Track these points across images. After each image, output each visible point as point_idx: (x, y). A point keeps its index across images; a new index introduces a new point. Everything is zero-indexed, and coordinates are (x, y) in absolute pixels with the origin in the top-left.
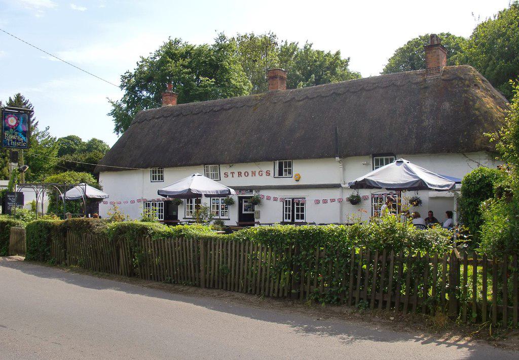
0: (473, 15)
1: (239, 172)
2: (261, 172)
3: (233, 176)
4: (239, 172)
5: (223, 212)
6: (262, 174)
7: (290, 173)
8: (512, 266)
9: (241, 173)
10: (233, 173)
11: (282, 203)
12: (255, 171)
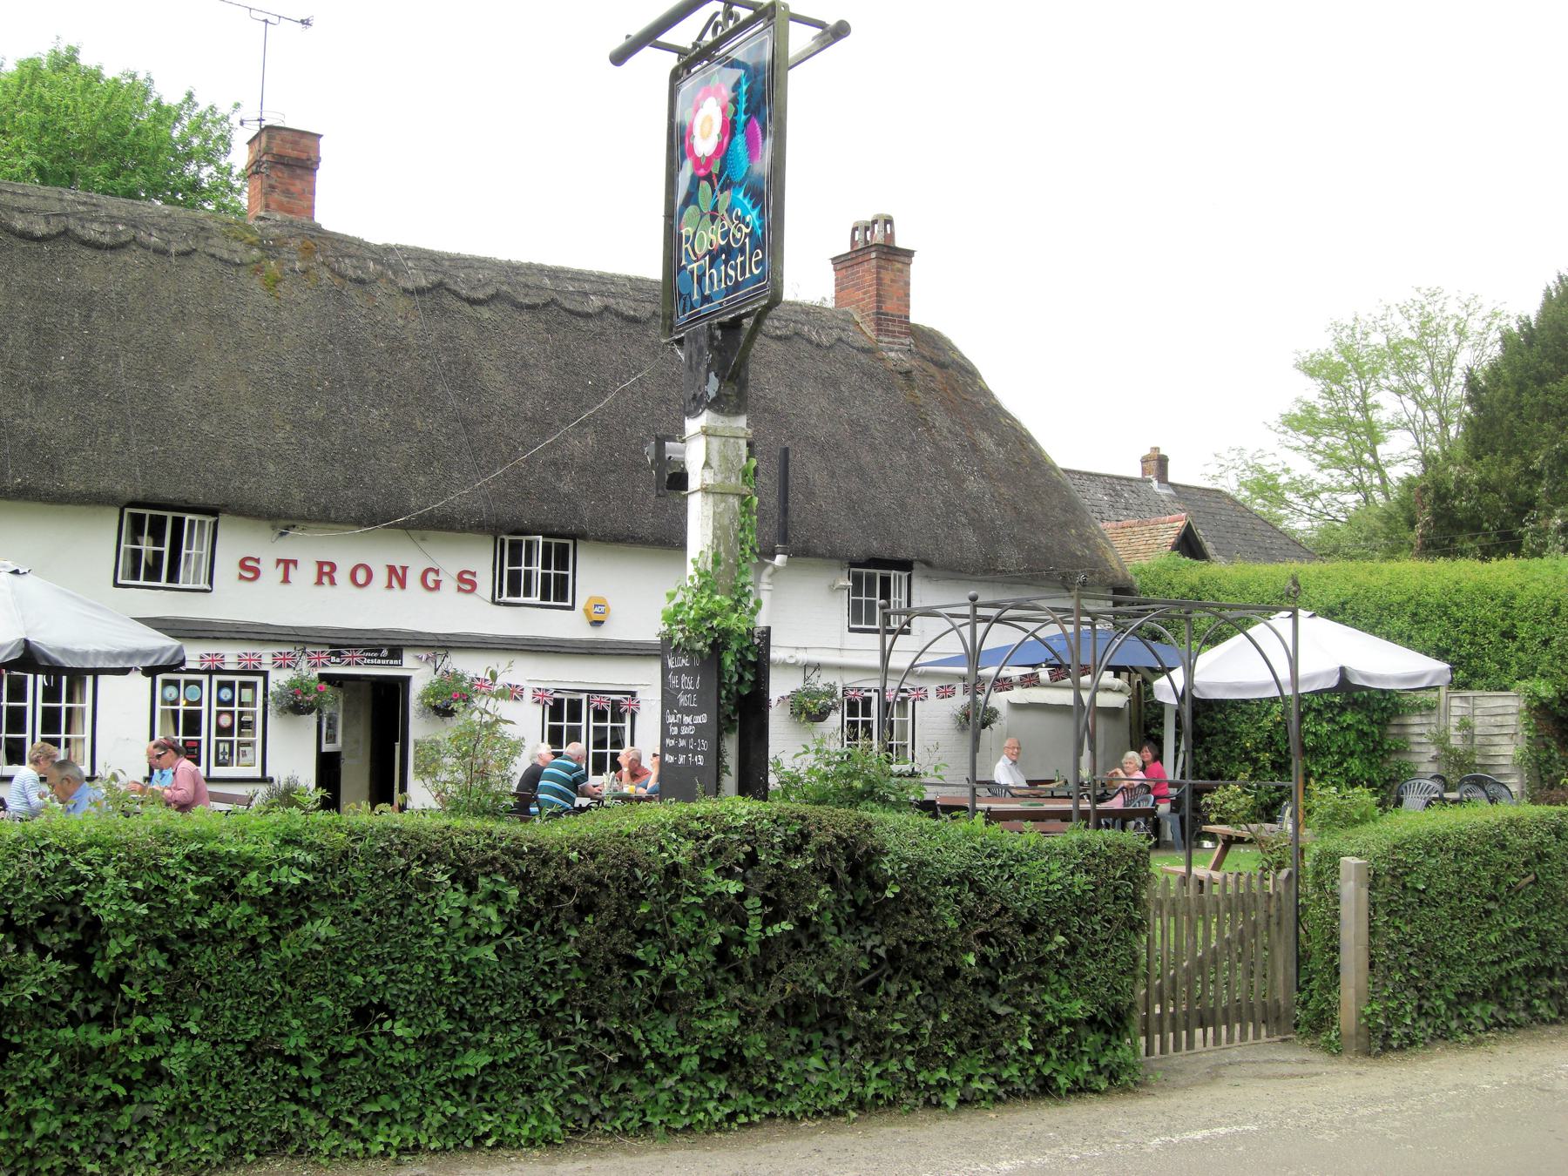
0: (305, 22)
1: (321, 564)
2: (431, 577)
3: (286, 580)
4: (321, 564)
5: (224, 747)
6: (438, 583)
7: (561, 594)
8: (393, 1110)
9: (333, 567)
10: (287, 564)
11: (541, 708)
12: (404, 569)
